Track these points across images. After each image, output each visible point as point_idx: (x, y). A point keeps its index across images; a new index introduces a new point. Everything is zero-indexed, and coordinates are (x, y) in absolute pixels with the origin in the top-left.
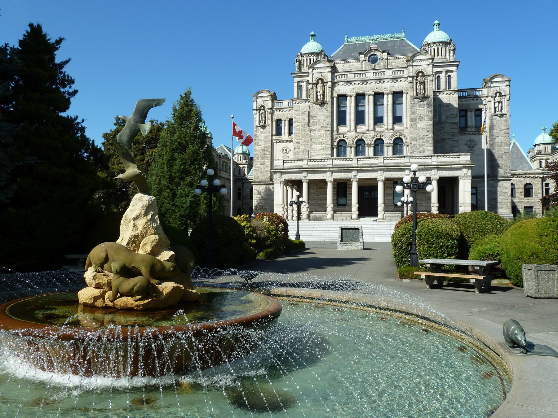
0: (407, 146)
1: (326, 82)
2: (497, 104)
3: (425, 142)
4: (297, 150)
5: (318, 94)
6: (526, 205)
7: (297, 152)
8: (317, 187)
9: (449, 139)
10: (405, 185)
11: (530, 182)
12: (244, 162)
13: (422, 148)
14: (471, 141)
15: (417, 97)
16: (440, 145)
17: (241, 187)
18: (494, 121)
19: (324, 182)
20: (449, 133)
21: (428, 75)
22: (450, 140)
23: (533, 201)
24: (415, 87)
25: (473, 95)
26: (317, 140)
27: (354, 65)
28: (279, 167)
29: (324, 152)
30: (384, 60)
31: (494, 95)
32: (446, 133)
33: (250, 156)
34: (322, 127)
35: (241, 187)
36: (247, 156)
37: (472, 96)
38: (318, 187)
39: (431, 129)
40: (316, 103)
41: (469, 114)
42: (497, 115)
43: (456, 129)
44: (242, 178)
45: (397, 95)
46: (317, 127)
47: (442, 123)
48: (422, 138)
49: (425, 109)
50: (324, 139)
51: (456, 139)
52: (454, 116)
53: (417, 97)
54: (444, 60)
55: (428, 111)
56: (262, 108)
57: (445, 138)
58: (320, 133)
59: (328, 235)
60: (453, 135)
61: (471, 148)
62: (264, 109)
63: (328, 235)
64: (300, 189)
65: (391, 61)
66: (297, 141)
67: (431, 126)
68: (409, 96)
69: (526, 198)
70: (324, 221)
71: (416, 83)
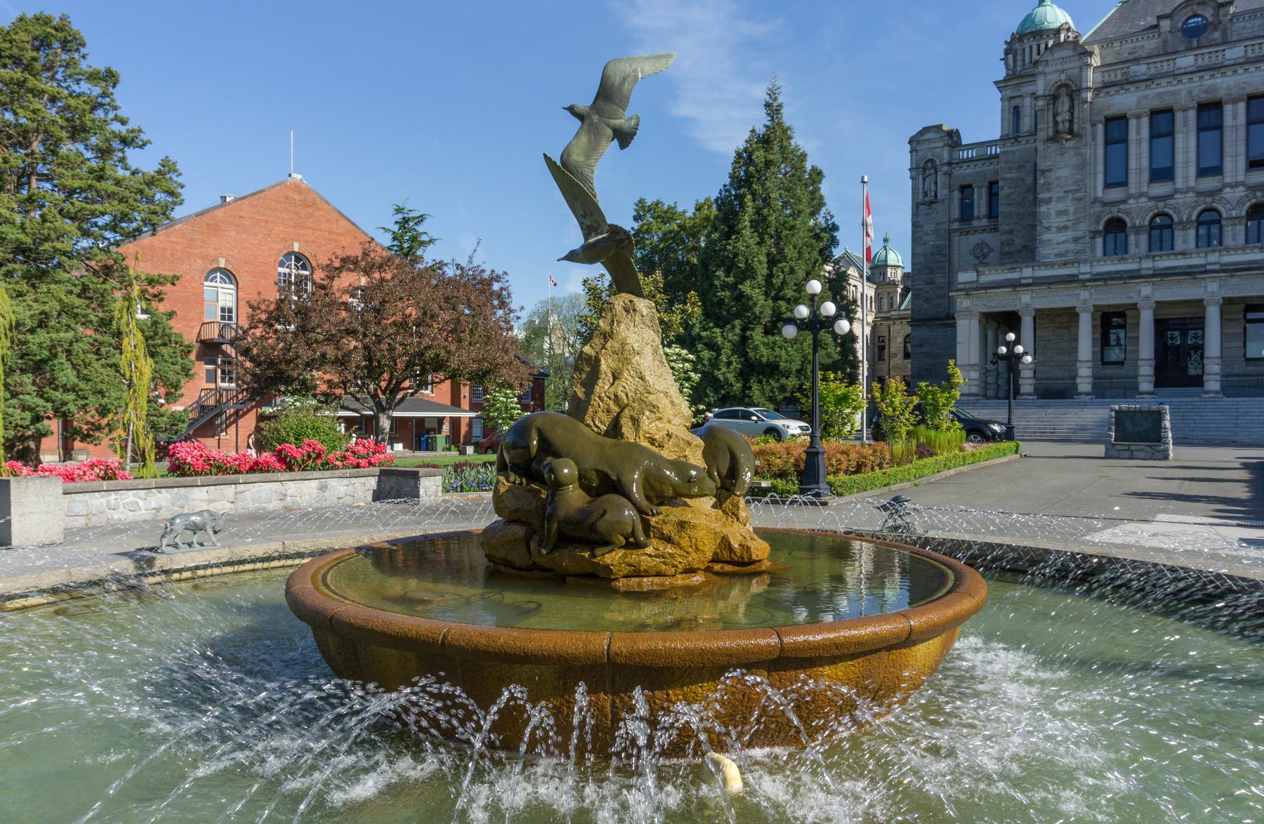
4: (1006, 249)
5: (1059, 119)
7: (1008, 253)
19: (1070, 315)
26: (1056, 221)
29: (1071, 246)
34: (1065, 192)
46: (1055, 194)
58: (1061, 206)
70: (1072, 398)
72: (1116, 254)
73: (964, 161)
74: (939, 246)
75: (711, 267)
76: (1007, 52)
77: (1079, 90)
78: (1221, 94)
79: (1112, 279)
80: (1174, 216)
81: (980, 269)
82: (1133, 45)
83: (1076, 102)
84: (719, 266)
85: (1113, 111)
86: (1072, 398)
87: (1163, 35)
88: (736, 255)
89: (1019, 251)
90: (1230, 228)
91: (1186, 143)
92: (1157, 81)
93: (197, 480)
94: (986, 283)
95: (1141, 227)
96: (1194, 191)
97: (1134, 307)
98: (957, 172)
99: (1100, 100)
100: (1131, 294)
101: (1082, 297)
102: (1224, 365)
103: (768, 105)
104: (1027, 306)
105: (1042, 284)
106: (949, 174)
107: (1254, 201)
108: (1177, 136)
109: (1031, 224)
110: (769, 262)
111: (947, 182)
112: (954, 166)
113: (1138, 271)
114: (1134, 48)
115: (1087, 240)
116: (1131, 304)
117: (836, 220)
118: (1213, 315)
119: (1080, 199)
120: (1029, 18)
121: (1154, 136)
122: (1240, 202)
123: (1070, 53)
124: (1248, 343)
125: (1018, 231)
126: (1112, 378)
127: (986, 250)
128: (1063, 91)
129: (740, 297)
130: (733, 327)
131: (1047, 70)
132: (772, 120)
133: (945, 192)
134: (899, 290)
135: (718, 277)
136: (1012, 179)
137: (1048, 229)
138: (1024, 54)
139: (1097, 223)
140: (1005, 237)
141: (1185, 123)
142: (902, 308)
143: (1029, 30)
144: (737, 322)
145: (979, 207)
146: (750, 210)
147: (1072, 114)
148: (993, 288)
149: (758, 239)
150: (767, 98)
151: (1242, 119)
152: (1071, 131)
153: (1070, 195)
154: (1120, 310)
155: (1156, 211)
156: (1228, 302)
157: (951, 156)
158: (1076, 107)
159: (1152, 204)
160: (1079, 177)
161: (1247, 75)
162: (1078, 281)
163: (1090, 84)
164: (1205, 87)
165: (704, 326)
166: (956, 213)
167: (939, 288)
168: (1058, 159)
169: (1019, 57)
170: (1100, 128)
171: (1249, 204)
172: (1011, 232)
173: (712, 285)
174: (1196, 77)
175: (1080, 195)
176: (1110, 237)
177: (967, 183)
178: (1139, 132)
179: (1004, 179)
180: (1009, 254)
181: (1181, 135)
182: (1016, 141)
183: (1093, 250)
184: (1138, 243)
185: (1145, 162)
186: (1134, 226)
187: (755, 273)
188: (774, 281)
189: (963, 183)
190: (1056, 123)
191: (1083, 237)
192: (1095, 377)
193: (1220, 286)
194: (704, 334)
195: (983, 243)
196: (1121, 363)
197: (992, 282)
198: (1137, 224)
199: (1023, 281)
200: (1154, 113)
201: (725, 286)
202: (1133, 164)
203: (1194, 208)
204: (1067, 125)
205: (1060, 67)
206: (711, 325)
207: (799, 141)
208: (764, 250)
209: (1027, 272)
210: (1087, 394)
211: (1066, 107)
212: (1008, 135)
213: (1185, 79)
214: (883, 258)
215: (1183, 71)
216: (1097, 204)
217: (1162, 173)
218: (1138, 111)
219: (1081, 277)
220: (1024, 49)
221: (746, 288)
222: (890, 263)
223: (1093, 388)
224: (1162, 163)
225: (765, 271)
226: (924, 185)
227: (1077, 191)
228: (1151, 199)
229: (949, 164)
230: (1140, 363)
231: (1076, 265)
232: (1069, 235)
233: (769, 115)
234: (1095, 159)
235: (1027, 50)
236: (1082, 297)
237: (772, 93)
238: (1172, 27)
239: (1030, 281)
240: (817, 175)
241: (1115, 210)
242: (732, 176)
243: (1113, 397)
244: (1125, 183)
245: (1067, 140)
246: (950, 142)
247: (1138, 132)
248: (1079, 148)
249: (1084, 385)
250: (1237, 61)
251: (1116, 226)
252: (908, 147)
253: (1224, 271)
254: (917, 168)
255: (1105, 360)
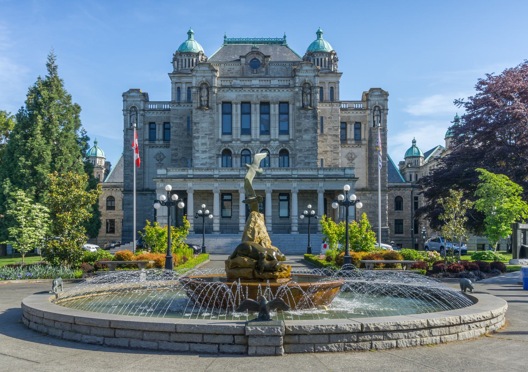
3: (311, 154)
4: (174, 158)
5: (202, 99)
6: (396, 218)
7: (175, 160)
8: (304, 198)
11: (110, 193)
19: (210, 194)
26: (201, 148)
27: (235, 69)
34: (206, 134)
37: (352, 109)
38: (203, 198)
41: (349, 126)
45: (284, 105)
46: (201, 134)
48: (307, 150)
55: (314, 123)
56: (377, 109)
58: (204, 141)
64: (289, 200)
69: (396, 211)
72: (227, 166)
75: (15, 155)
76: (174, 59)
77: (211, 87)
78: (269, 99)
79: (228, 178)
80: (251, 151)
81: (168, 168)
83: (210, 92)
84: (21, 155)
85: (226, 99)
86: (211, 233)
87: (242, 65)
88: (32, 149)
89: (181, 159)
90: (273, 159)
91: (256, 118)
92: (244, 89)
94: (171, 176)
95: (238, 154)
96: (259, 141)
97: (237, 191)
98: (148, 115)
99: (220, 93)
100: (236, 186)
101: (215, 186)
103: (48, 65)
104: (191, 188)
105: (198, 178)
107: (282, 148)
108: (252, 115)
109: (189, 148)
110: (52, 155)
111: (142, 120)
113: (239, 175)
114: (230, 68)
115: (215, 158)
116: (236, 190)
117: (88, 134)
118: (269, 197)
119: (212, 139)
120: (184, 45)
121: (242, 113)
122: (277, 148)
123: (207, 69)
124: (280, 210)
126: (226, 224)
127: (162, 157)
128: (204, 86)
129: (35, 173)
130: (31, 190)
131: (197, 75)
132: (51, 73)
133: (142, 124)
134: (103, 171)
135: (21, 161)
137: (198, 151)
138: (182, 62)
139: (219, 150)
140: (174, 152)
141: (255, 110)
142: (105, 181)
143: (185, 51)
144: (34, 188)
145: (159, 135)
146: (40, 124)
147: (208, 98)
148: (175, 178)
149: (46, 141)
150: (48, 60)
152: (208, 106)
154: (230, 192)
155: (244, 148)
156: (274, 191)
157: (144, 106)
158: (210, 95)
159: (242, 144)
160: (211, 128)
161: (279, 93)
162: (213, 178)
163: (216, 85)
164: (263, 95)
165: (11, 189)
166: (147, 137)
168: (202, 118)
169: (180, 63)
170: (220, 106)
171: (280, 149)
172: (176, 149)
173: (16, 165)
174: (260, 90)
175: (212, 136)
176: (225, 158)
177: (153, 121)
178: (237, 110)
179: (173, 123)
180: (176, 160)
181: (254, 115)
183: (217, 163)
184: (236, 162)
185: (239, 125)
186: (235, 154)
187: (44, 160)
188: (56, 166)
189: (151, 121)
190: (201, 101)
191: (214, 157)
192: (221, 224)
193: (271, 185)
194: (11, 193)
197: (174, 175)
199: (189, 176)
200: (243, 103)
201: (25, 167)
202: (234, 125)
204: (206, 102)
205: (203, 75)
206: (17, 188)
207: (68, 88)
208: (50, 148)
209: (190, 172)
210: (218, 231)
211: (206, 94)
212: (175, 101)
213: (255, 90)
214: (94, 152)
215: (254, 86)
216: (219, 142)
217: (246, 131)
218: (237, 101)
219: (215, 176)
221: (39, 168)
222: (98, 155)
223: (220, 229)
224: (246, 126)
225: (50, 160)
226: (130, 119)
227: (210, 134)
228: (242, 142)
229: (144, 110)
230: (240, 217)
231: (212, 170)
233: (49, 70)
234: (218, 121)
235: (184, 61)
236: (215, 186)
237: (51, 59)
238: (246, 62)
239: (192, 176)
240: (77, 109)
241: (227, 145)
242: (27, 102)
243: (227, 233)
244: (231, 134)
245: (206, 110)
246: (144, 99)
248: (211, 114)
249: (216, 227)
250: (275, 86)
251: (227, 153)
252: (122, 98)
253: (273, 178)
254: (127, 110)
255: (224, 215)
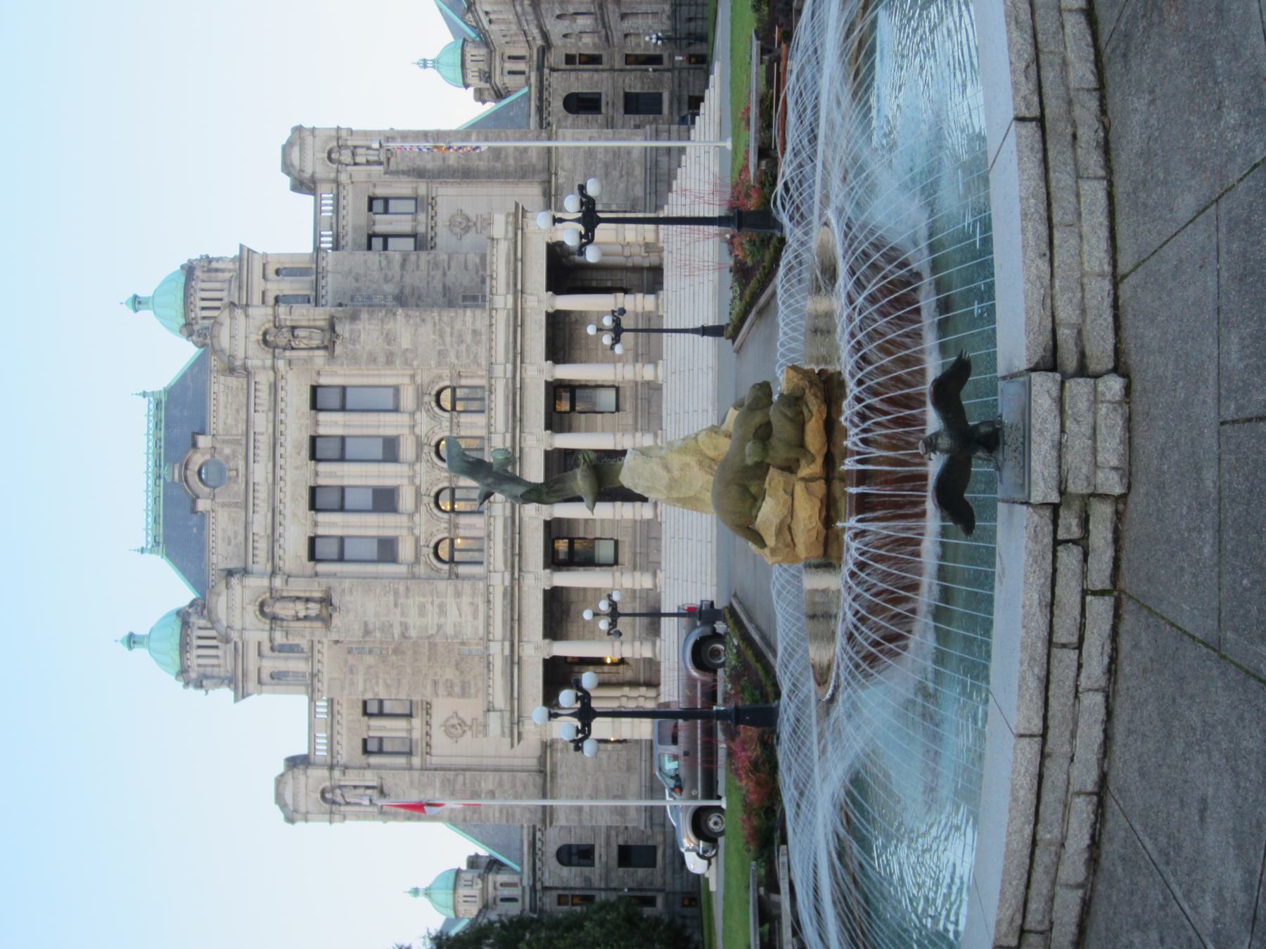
0: (459, 375)
1: (271, 593)
2: (358, 159)
4: (457, 689)
5: (302, 614)
6: (622, 111)
7: (463, 688)
9: (444, 274)
10: (584, 241)
12: (480, 886)
13: (469, 338)
14: (451, 224)
15: (329, 347)
16: (460, 299)
17: (555, 893)
18: (402, 167)
20: (428, 275)
21: (275, 317)
22: (448, 273)
23: (611, 92)
24: (304, 354)
25: (331, 217)
26: (432, 619)
28: (507, 723)
29: (466, 600)
30: (218, 446)
31: (335, 166)
32: (428, 283)
33: (464, 867)
34: (396, 606)
35: (555, 893)
36: (462, 875)
39: (418, 314)
40: (326, 620)
41: (379, 228)
42: (388, 159)
43: (418, 257)
44: (527, 891)
46: (396, 619)
47: (402, 292)
48: (441, 336)
49: (364, 328)
50: (430, 599)
51: (445, 257)
52: (384, 263)
53: (329, 347)
54: (234, 285)
55: (369, 319)
57: (441, 285)
58: (413, 612)
59: (699, 577)
60: (436, 265)
61: (471, 224)
62: (332, 789)
63: (699, 577)
65: (221, 426)
66: (429, 688)
67: (410, 313)
68: (327, 367)
69: (603, 110)
70: (659, 595)
71: (293, 349)
73: (331, 749)
74: (442, 782)
76: (199, 685)
82: (220, 541)
83: (285, 594)
89: (462, 673)
93: (783, 863)
95: (450, 522)
102: (624, 431)
106: (346, 768)
111: (355, 772)
112: (335, 762)
125: (436, 674)
136: (365, 681)
138: (205, 666)
140: (441, 690)
141: (332, 475)
147: (298, 598)
151: (339, 417)
153: (401, 601)
159: (423, 509)
167: (500, 784)
169: (209, 670)
174: (280, 461)
179: (365, 690)
182: (316, 675)
190: (306, 618)
195: (444, 725)
196: (616, 543)
198: (446, 525)
200: (313, 506)
203: (434, 465)
220: (199, 665)
231: (491, 589)
232: (450, 602)
235: (202, 661)
241: (425, 551)
247: (334, 525)
254: (331, 812)
